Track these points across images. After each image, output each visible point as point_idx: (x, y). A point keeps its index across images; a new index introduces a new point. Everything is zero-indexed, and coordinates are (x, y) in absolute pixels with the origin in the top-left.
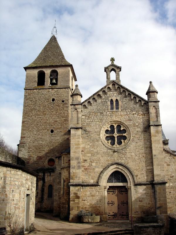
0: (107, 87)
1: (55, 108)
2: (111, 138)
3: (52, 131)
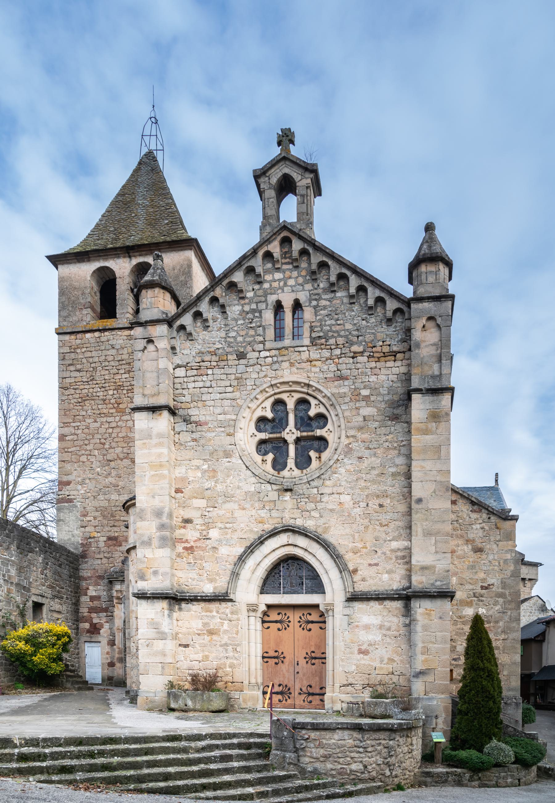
0: (261, 253)
2: (272, 448)
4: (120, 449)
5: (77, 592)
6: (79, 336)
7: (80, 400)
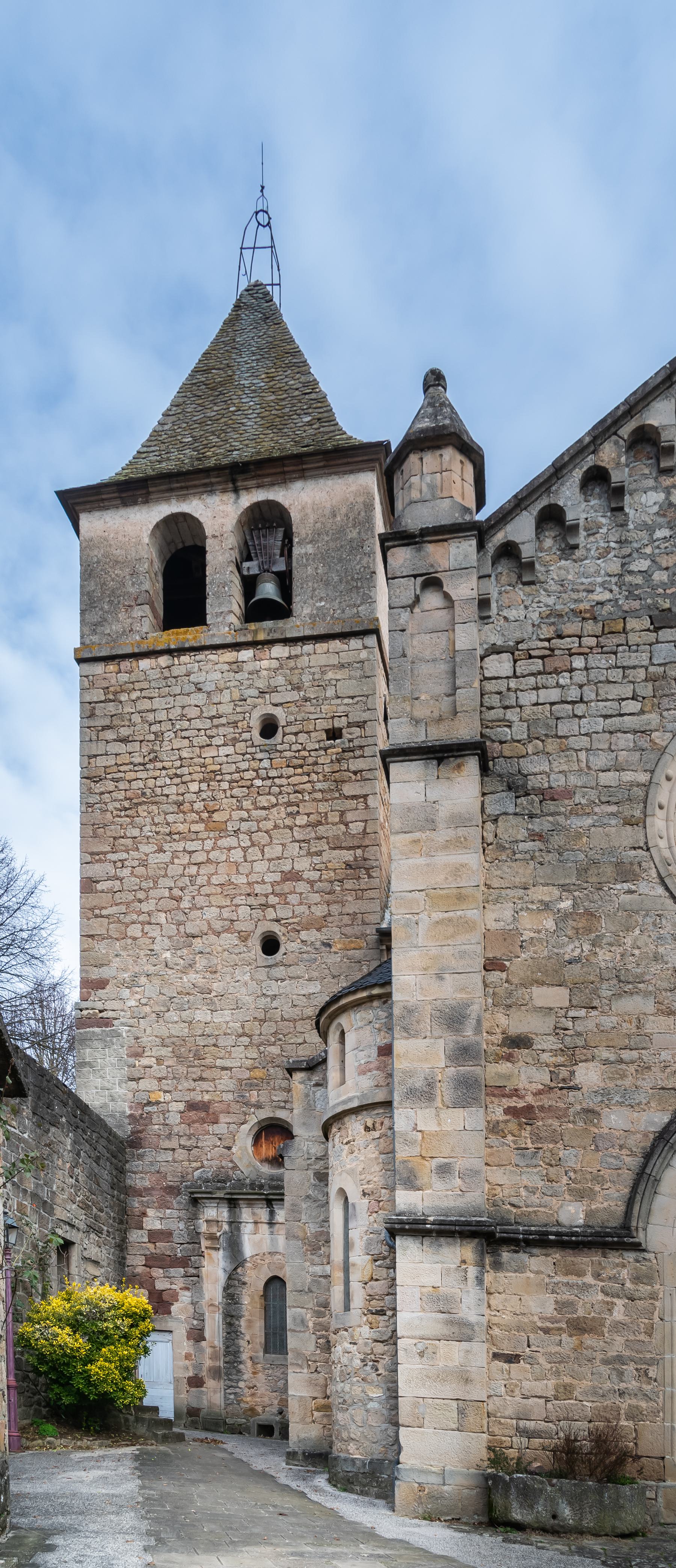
1: (284, 781)
3: (270, 945)
4: (215, 911)
5: (125, 1220)
6: (126, 664)
7: (126, 804)
